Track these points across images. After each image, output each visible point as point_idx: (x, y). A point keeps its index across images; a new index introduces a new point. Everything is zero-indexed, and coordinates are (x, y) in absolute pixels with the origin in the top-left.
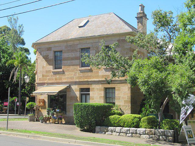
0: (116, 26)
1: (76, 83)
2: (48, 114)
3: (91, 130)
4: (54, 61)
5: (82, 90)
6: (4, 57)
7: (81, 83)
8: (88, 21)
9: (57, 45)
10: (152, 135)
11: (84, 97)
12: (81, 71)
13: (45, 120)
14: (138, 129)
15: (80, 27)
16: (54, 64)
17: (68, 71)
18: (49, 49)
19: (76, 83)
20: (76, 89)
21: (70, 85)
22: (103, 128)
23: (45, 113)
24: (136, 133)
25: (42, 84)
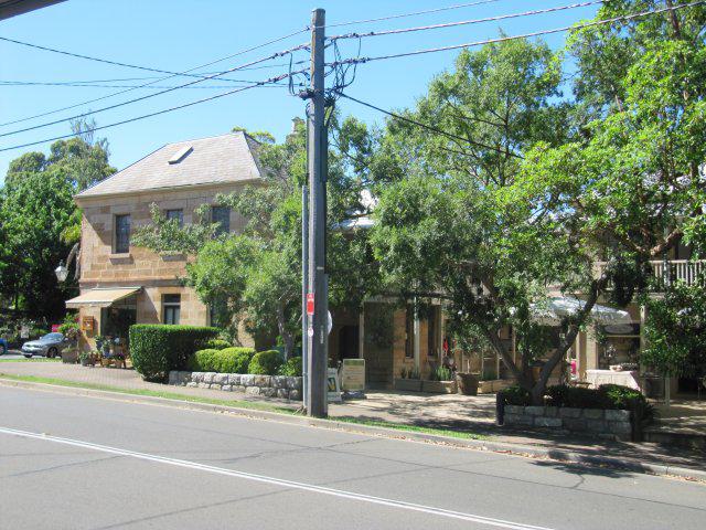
0: (236, 164)
1: (155, 283)
2: (99, 347)
3: (164, 380)
4: (115, 236)
5: (167, 298)
6: (58, 217)
7: (165, 283)
8: (191, 150)
9: (121, 201)
10: (265, 386)
11: (170, 312)
12: (167, 259)
13: (91, 361)
14: (244, 376)
15: (171, 163)
16: (114, 241)
17: (141, 257)
18: (105, 210)
19: (155, 283)
20: (154, 294)
21: (143, 288)
22: (182, 374)
23: (92, 343)
24: (239, 384)
25: (91, 285)
